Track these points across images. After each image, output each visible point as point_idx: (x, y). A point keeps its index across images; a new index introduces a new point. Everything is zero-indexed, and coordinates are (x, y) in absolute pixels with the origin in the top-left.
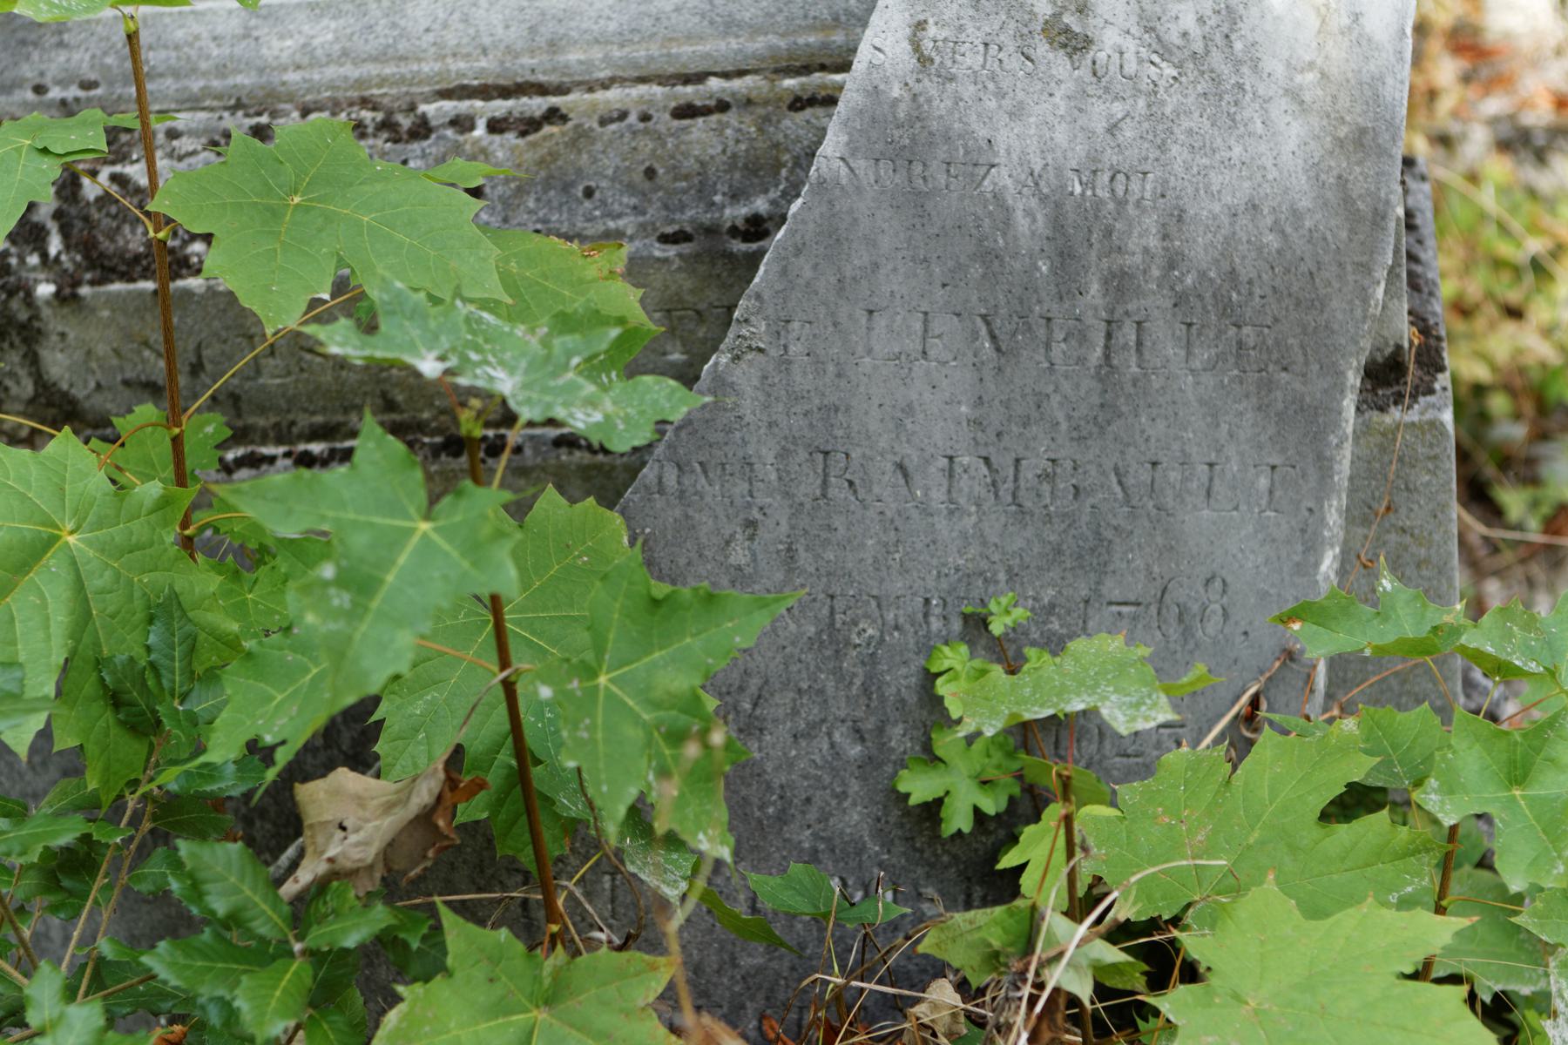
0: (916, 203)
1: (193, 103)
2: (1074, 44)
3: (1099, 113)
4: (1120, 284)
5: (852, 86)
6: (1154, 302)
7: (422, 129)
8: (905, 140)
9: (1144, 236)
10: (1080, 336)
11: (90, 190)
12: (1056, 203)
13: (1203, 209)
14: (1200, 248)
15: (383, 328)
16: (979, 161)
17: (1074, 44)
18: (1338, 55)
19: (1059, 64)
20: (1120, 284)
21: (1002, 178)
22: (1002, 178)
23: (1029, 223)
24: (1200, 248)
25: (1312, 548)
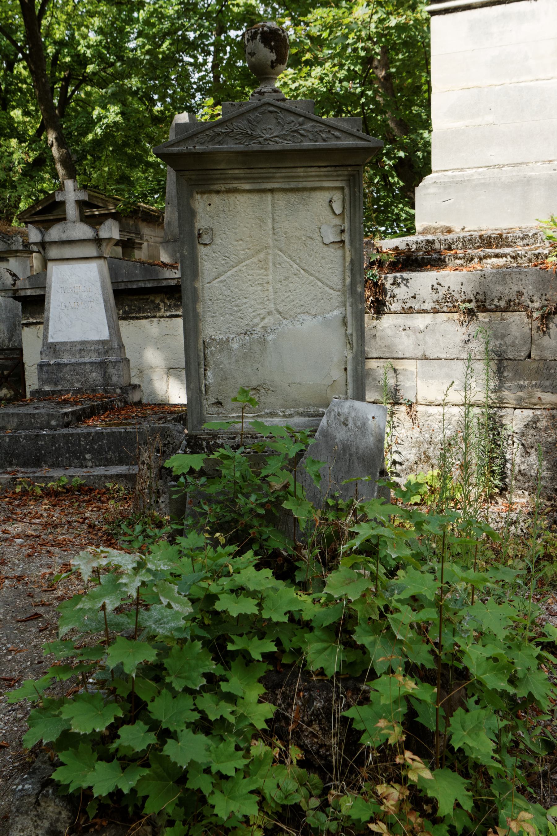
0: (327, 442)
1: (225, 433)
2: (346, 425)
3: (349, 434)
4: (351, 455)
5: (319, 428)
6: (355, 458)
7: (257, 437)
8: (326, 435)
9: (354, 450)
10: (346, 461)
11: (211, 443)
12: (343, 444)
13: (361, 447)
14: (360, 452)
15: (170, 548)
16: (334, 438)
17: (346, 425)
18: (377, 430)
19: (344, 427)
20: (351, 455)
21: (337, 440)
22: (337, 440)
23: (340, 446)
24: (360, 452)
25: (374, 492)
